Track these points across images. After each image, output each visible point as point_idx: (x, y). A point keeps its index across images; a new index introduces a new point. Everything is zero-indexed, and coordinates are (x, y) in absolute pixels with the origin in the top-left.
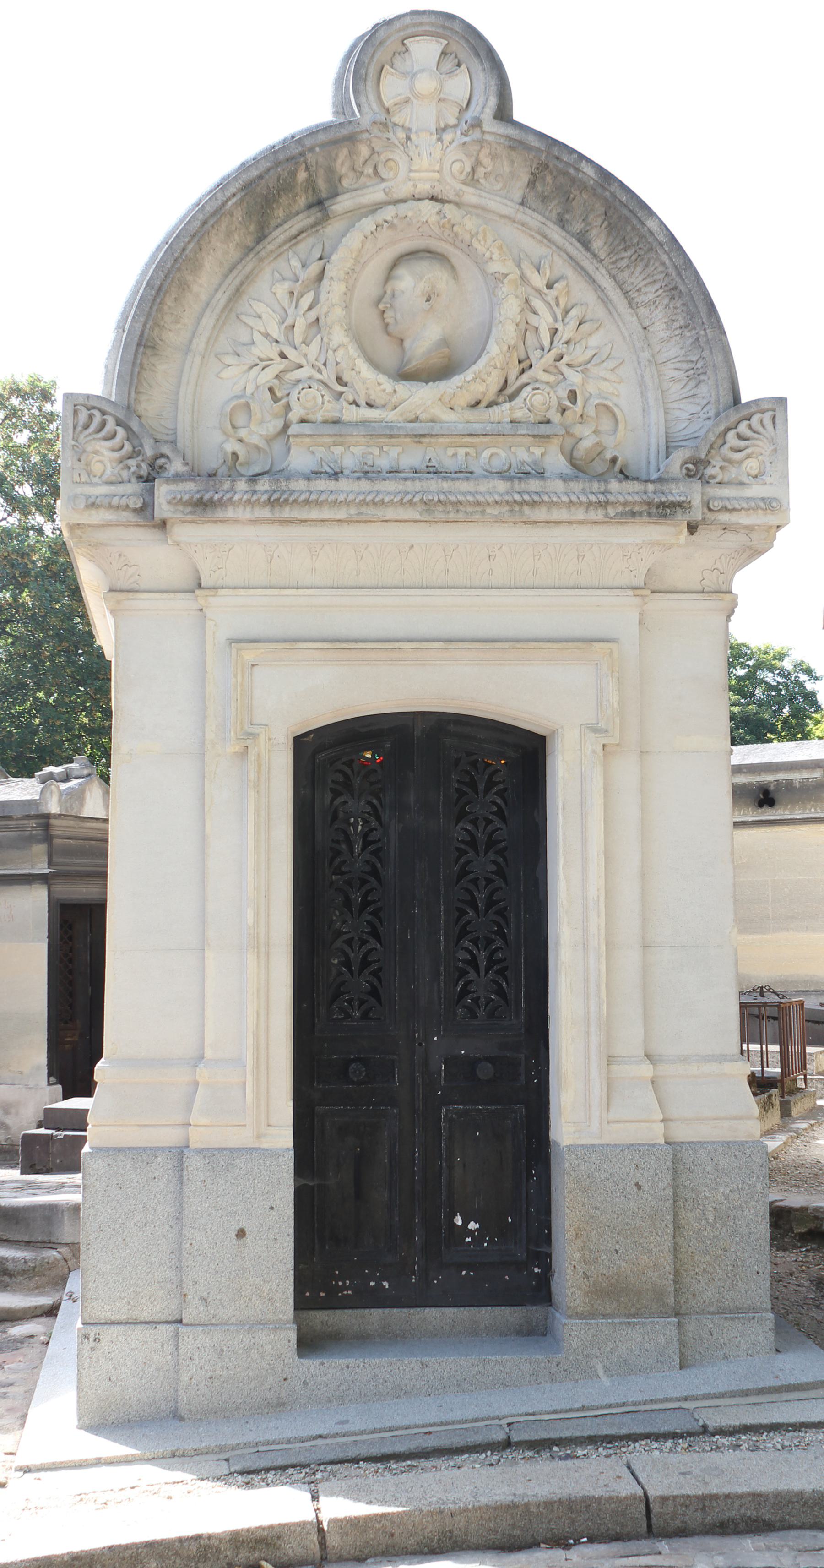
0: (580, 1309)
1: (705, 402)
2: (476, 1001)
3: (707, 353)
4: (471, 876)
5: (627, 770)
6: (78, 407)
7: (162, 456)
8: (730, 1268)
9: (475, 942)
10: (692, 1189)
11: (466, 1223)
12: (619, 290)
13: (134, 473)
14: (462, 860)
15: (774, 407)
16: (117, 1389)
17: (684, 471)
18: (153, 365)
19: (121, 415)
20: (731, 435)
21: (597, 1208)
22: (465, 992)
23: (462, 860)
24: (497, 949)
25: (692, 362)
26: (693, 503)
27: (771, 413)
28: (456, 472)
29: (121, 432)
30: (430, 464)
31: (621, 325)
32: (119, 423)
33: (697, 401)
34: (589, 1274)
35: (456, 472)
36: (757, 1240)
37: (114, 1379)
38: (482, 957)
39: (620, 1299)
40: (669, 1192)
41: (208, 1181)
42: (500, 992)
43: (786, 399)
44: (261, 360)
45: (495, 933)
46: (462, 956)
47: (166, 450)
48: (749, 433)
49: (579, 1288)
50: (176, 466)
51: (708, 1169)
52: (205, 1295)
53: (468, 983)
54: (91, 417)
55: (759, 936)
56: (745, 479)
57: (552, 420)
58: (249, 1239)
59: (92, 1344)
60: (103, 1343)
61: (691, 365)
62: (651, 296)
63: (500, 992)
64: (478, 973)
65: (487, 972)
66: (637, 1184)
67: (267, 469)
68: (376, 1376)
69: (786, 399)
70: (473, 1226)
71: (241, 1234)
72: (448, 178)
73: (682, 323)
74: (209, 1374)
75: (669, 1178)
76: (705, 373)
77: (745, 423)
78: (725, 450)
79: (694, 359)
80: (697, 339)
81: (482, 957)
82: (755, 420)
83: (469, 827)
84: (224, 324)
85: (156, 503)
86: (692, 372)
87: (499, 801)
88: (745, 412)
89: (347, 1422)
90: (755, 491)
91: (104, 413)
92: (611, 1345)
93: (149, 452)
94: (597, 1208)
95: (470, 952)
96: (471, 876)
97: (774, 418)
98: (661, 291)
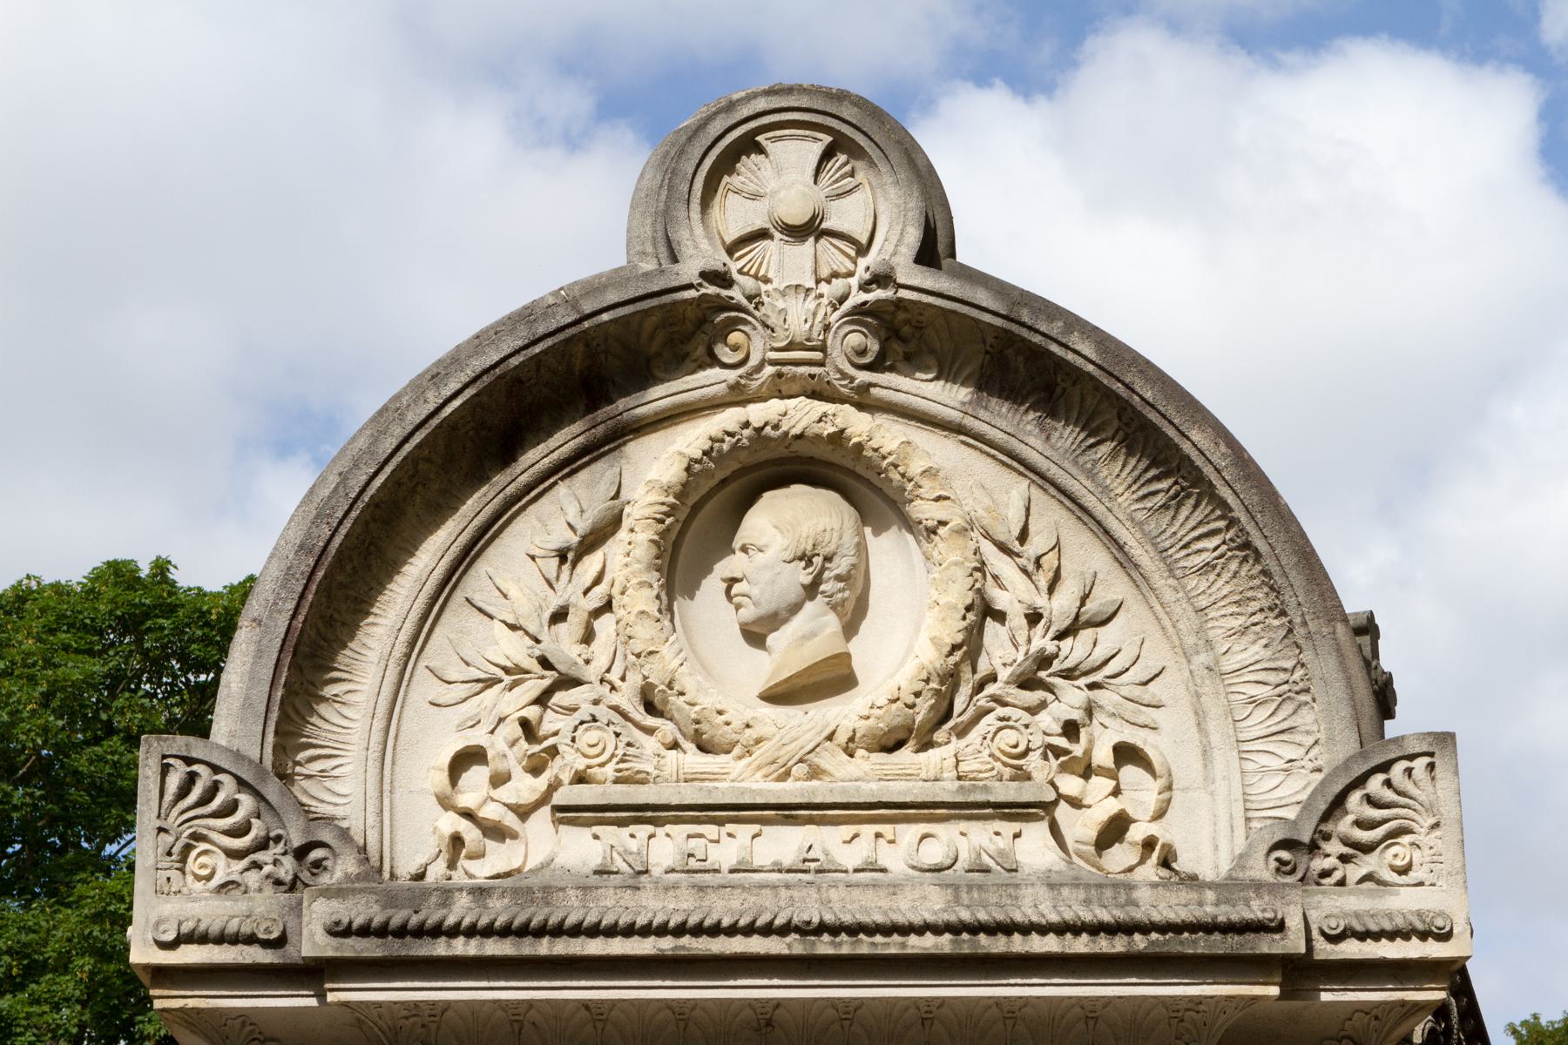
1: (1310, 740)
3: (1306, 656)
6: (171, 761)
12: (1149, 547)
13: (268, 877)
15: (1431, 750)
17: (1273, 864)
18: (313, 684)
20: (1355, 798)
25: (1285, 670)
26: (1288, 923)
27: (1427, 760)
28: (856, 871)
29: (246, 802)
30: (811, 855)
31: (1158, 607)
32: (242, 784)
33: (1298, 738)
35: (856, 871)
43: (1452, 736)
44: (507, 670)
47: (325, 835)
48: (1389, 795)
50: (344, 867)
54: (192, 778)
57: (1034, 775)
61: (1283, 676)
67: (516, 865)
69: (1452, 736)
73: (1266, 603)
76: (1307, 691)
77: (1380, 777)
78: (1345, 826)
79: (1289, 664)
80: (1290, 631)
82: (1397, 770)
85: (305, 932)
86: (1286, 687)
91: (216, 770)
98: (1224, 548)
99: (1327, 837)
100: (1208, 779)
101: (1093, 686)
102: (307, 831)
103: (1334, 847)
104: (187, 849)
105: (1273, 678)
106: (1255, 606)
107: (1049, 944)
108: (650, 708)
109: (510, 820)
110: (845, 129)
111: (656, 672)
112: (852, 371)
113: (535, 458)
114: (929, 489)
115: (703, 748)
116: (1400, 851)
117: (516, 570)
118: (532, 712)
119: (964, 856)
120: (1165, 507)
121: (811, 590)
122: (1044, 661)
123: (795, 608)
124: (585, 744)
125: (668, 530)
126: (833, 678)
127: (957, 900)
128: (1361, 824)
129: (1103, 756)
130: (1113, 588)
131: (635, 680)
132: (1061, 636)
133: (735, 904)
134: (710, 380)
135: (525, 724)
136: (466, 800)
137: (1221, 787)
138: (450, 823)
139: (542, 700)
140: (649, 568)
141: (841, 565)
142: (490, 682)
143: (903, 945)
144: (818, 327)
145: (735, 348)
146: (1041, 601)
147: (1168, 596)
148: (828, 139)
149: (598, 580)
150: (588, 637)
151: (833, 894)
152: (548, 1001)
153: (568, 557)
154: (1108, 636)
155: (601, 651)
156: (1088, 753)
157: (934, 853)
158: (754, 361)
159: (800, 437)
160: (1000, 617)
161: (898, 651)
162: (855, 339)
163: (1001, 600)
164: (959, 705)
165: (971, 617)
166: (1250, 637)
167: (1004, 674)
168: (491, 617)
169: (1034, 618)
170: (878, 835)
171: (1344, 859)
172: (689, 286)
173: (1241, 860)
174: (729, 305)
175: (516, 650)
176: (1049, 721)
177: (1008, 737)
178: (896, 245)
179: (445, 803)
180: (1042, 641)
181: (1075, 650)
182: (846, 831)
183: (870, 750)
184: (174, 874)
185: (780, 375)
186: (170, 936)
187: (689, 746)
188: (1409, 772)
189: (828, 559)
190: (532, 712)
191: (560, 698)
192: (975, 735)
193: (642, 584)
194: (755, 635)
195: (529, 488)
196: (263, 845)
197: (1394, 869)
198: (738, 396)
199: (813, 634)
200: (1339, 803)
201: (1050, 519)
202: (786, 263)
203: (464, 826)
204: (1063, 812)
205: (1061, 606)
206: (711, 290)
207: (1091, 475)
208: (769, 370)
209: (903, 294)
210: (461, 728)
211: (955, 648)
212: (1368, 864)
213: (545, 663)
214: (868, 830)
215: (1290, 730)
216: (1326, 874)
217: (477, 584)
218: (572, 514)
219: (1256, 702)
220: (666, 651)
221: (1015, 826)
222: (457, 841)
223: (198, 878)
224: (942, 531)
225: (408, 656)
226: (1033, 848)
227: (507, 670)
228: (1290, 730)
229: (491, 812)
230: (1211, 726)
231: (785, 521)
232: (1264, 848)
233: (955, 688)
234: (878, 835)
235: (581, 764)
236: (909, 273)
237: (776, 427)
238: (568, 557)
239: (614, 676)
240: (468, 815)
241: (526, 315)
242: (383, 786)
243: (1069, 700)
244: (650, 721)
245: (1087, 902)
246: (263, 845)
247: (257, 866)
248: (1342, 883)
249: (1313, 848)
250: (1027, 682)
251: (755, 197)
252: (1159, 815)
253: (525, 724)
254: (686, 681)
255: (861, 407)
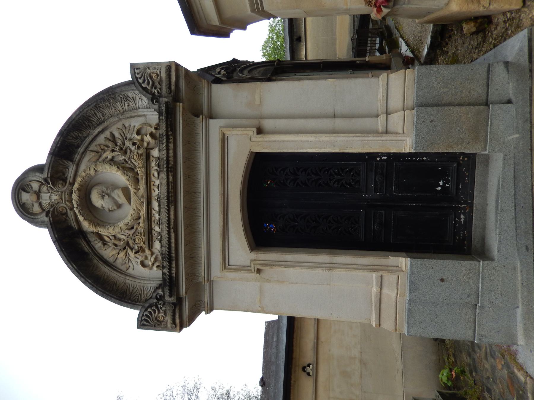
0: (483, 146)
2: (353, 180)
4: (307, 181)
5: (268, 124)
7: (156, 296)
8: (469, 81)
9: (331, 180)
10: (434, 98)
11: (440, 186)
14: (301, 184)
16: (503, 330)
19: (144, 310)
21: (440, 138)
22: (350, 184)
23: (301, 184)
24: (334, 172)
29: (149, 310)
32: (146, 310)
34: (467, 142)
36: (458, 70)
37: (498, 330)
38: (337, 177)
39: (479, 131)
40: (435, 108)
41: (421, 292)
42: (350, 171)
44: (126, 256)
45: (328, 172)
46: (336, 185)
47: (154, 295)
48: (142, 78)
49: (474, 146)
51: (426, 91)
52: (466, 295)
53: (347, 184)
54: (145, 320)
55: (337, 41)
56: (159, 79)
58: (444, 277)
59: (484, 337)
60: (483, 333)
62: (100, 115)
63: (350, 171)
64: (342, 179)
65: (343, 176)
66: (431, 122)
68: (505, 230)
70: (441, 183)
71: (442, 280)
72: (65, 189)
73: (108, 103)
74: (500, 296)
75: (429, 108)
77: (139, 80)
78: (149, 88)
81: (337, 177)
82: (138, 76)
83: (289, 181)
84: (116, 267)
87: (280, 170)
88: (135, 80)
89: (527, 247)
90: (163, 75)
91: (143, 315)
92: (499, 133)
93: (155, 301)
94: (440, 138)
95: (335, 182)
96: (307, 181)
97: (137, 69)
99: (151, 92)
100: (144, 116)
101: (126, 139)
102: (154, 299)
103: (153, 90)
104: (158, 321)
105: (123, 102)
106: (109, 105)
107: (171, 152)
108: (132, 228)
109: (154, 256)
110: (18, 187)
111: (124, 228)
112: (66, 186)
113: (86, 249)
114: (88, 172)
115: (139, 218)
116: (154, 76)
117: (109, 253)
118: (134, 251)
119: (156, 168)
120: (91, 123)
121: (109, 195)
122: (121, 149)
123: (113, 198)
124: (140, 241)
125: (98, 224)
126: (126, 191)
127: (163, 171)
128: (148, 84)
129: (139, 137)
130: (107, 134)
131: (127, 231)
132: (116, 145)
133: (164, 216)
134: (70, 214)
135: (136, 253)
136: (150, 264)
137: (145, 113)
138: (155, 268)
139: (132, 249)
140: (105, 228)
141: (104, 189)
142: (129, 259)
143: (172, 182)
144: (57, 193)
145: (63, 209)
146: (110, 149)
147: (108, 123)
148: (21, 190)
149: (109, 238)
150: (120, 240)
151: (162, 196)
152: (185, 253)
153: (105, 243)
154: (117, 135)
155: (123, 237)
156: (138, 140)
157: (156, 174)
158: (65, 206)
159: (79, 197)
160: (113, 157)
161: (120, 178)
162: (60, 186)
163: (110, 157)
164: (130, 166)
165: (112, 164)
166: (116, 106)
167: (124, 158)
168: (117, 258)
169: (113, 151)
170: (153, 185)
171: (155, 88)
172: (49, 219)
173: (155, 110)
174: (53, 211)
175: (122, 254)
176: (133, 148)
177: (135, 157)
178: (40, 177)
179: (151, 268)
180: (117, 149)
181: (119, 142)
182: (153, 191)
183: (139, 185)
184: (163, 324)
185: (68, 201)
186: (174, 326)
187: (139, 221)
188: (138, 74)
189: (103, 192)
190: (134, 251)
191: (131, 245)
192: (136, 164)
193: (108, 230)
194: (119, 206)
195: (92, 250)
196: (157, 307)
197: (157, 77)
198: (72, 209)
199: (118, 195)
200: (145, 89)
201: (93, 147)
202: (46, 199)
203: (155, 265)
204: (150, 146)
205: (110, 144)
206: (50, 215)
207: (86, 138)
208: (67, 203)
209: (49, 176)
210: (138, 265)
211: (118, 168)
212: (157, 84)
213: (124, 248)
214: (152, 187)
215: (133, 98)
216: (158, 92)
217: (111, 260)
218: (96, 242)
219: (129, 105)
220: (120, 225)
221: (151, 157)
222: (158, 267)
223: (164, 319)
224: (96, 169)
225: (124, 274)
226: (155, 153)
227: (126, 256)
228: (133, 98)
229: (152, 260)
230: (133, 115)
231: (97, 200)
232: (153, 106)
233: (126, 168)
234: (153, 185)
235: (142, 243)
236: (45, 175)
237: (77, 202)
238: (105, 243)
239: (127, 235)
240: (153, 264)
241: (300, 80)
242: (149, 279)
243: (128, 144)
244: (135, 228)
245: (163, 144)
246: (157, 307)
247: (161, 308)
248: (160, 89)
249: (153, 94)
250: (125, 153)
251: (33, 205)
252: (151, 126)
253: (136, 253)
254: (126, 221)
255: (74, 184)
